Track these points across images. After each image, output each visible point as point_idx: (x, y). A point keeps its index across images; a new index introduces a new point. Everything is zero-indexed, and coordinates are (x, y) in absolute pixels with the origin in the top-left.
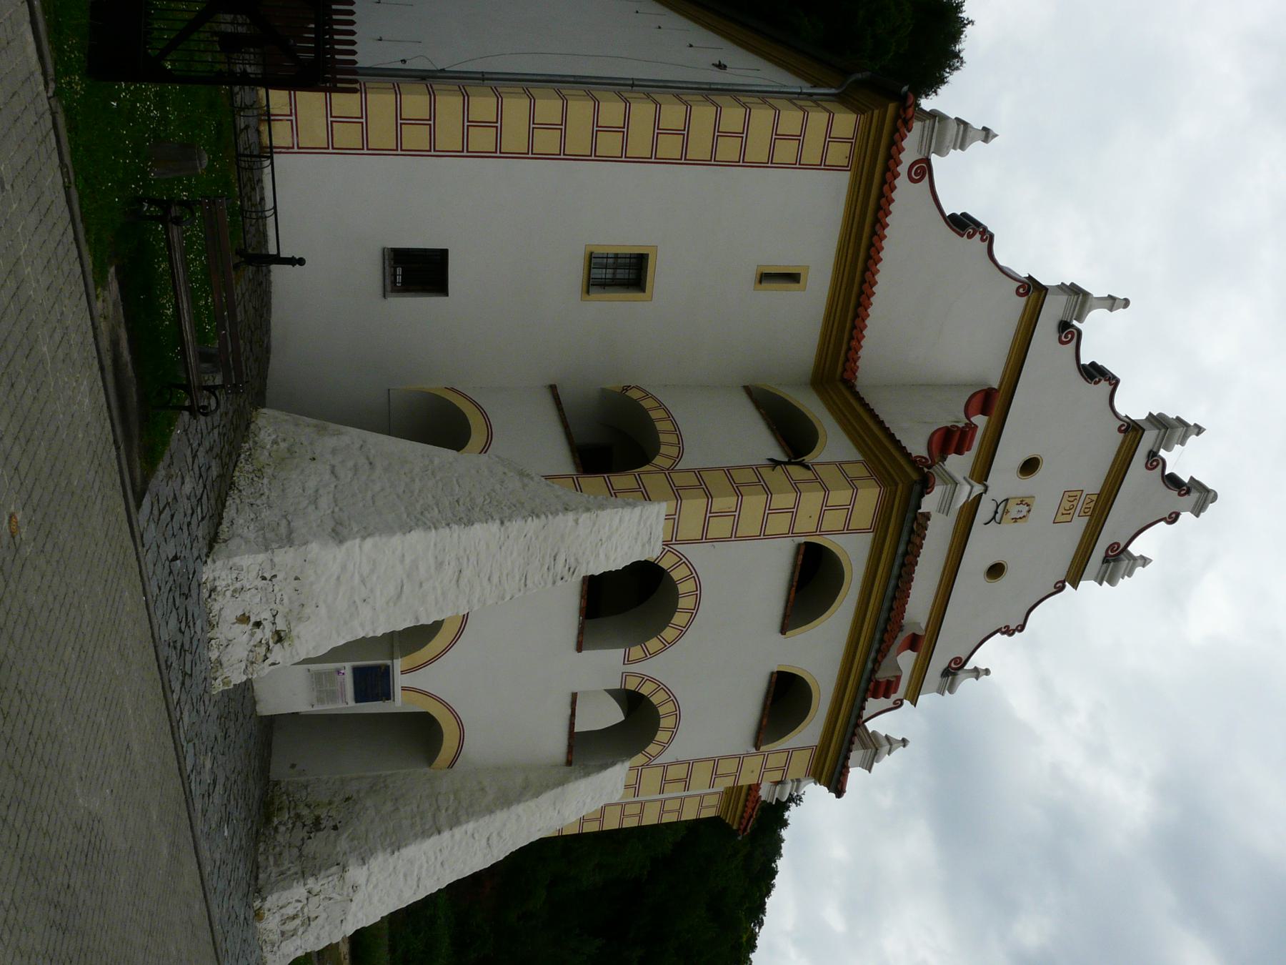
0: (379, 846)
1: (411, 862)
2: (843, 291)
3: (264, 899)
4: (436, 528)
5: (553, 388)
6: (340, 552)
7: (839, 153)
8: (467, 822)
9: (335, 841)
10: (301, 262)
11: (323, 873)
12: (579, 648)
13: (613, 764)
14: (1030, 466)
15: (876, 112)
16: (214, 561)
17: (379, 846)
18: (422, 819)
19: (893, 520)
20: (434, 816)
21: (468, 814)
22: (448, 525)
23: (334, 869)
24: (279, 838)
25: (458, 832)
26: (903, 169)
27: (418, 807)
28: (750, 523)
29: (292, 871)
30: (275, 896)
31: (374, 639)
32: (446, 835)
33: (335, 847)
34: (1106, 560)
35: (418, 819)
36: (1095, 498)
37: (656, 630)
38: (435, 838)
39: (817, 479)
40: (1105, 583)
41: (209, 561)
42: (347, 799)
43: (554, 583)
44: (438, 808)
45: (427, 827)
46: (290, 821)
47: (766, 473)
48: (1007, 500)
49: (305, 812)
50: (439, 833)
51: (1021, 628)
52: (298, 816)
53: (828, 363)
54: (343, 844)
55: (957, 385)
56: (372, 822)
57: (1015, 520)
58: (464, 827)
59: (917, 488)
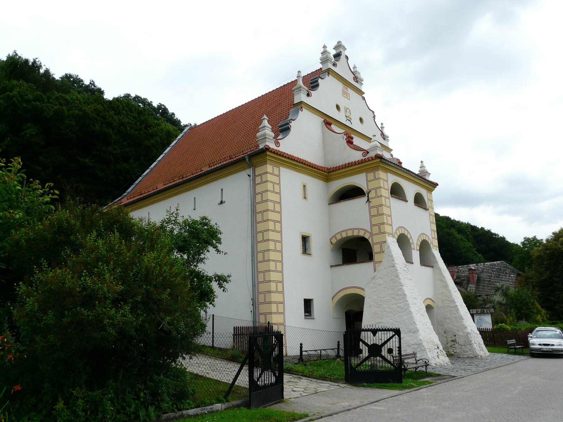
0: (461, 323)
1: (464, 314)
2: (307, 171)
3: (478, 355)
4: (409, 305)
5: (332, 266)
6: (421, 331)
7: (276, 171)
8: (453, 298)
9: (459, 336)
10: (301, 344)
11: (470, 339)
12: (413, 263)
13: (433, 254)
14: (338, 107)
15: (268, 158)
16: (432, 364)
17: (461, 323)
18: (452, 311)
19: (385, 167)
20: (451, 307)
21: (451, 298)
22: (407, 301)
23: (469, 336)
24: (458, 352)
25: (456, 301)
26: (278, 149)
27: (448, 312)
28: (275, 179)
29: (469, 348)
30: (477, 352)
31: (432, 322)
32: (457, 304)
33: (462, 336)
34: (357, 82)
35: (452, 312)
36: (344, 85)
37: (408, 240)
38: (458, 307)
39: (376, 189)
40: (362, 82)
41: (432, 365)
42: (445, 332)
43: (409, 271)
44: (448, 306)
45: (455, 309)
46: (453, 349)
47: (371, 205)
48: (346, 116)
49: (449, 344)
50: (457, 306)
51: (373, 112)
52: (451, 346)
53: (323, 177)
54: (461, 333)
55: (323, 132)
56: (453, 325)
57: (350, 113)
58: (455, 299)
59: (382, 160)
